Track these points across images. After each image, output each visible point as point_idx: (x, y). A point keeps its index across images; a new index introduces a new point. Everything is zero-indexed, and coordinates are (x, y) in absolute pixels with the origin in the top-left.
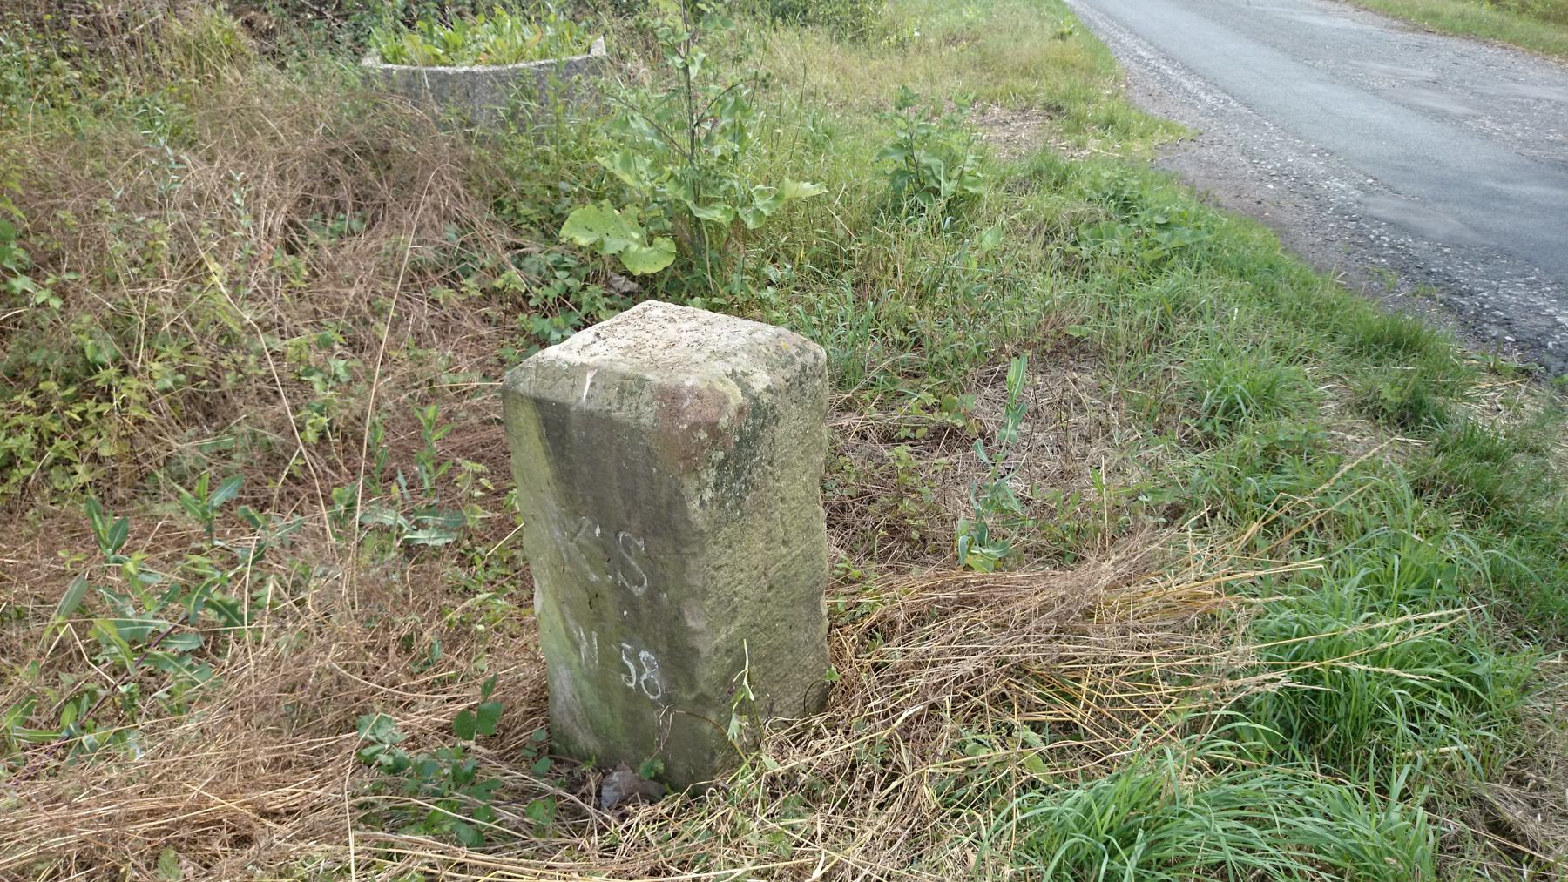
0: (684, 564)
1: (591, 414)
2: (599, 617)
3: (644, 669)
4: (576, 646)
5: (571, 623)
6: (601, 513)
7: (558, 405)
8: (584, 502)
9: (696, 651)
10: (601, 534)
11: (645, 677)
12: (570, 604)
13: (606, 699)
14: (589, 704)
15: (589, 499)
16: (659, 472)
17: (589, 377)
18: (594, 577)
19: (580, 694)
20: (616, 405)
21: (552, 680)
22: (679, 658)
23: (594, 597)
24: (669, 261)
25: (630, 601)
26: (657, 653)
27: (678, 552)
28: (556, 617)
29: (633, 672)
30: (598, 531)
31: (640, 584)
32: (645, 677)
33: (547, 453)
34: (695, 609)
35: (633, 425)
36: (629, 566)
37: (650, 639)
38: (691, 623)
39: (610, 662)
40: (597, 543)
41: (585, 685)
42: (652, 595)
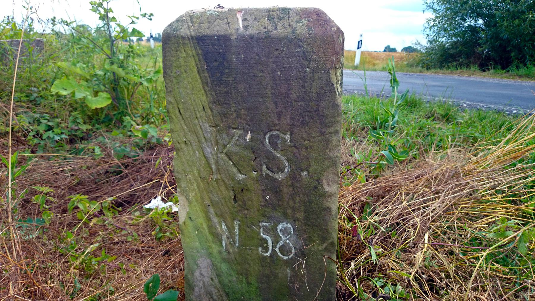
0: (327, 142)
1: (252, 37)
2: (244, 206)
3: (282, 237)
4: (217, 237)
5: (215, 220)
6: (256, 123)
7: (220, 37)
8: (239, 116)
9: (328, 210)
10: (251, 139)
11: (281, 243)
12: (213, 203)
13: (244, 273)
14: (226, 281)
15: (243, 112)
16: (312, 70)
17: (239, 16)
18: (240, 177)
19: (218, 275)
20: (270, 27)
21: (192, 272)
22: (312, 217)
23: (239, 193)
24: (109, 102)
25: (273, 187)
26: (294, 220)
27: (323, 134)
28: (201, 221)
29: (270, 243)
30: (249, 136)
31: (282, 170)
32: (281, 243)
33: (204, 83)
34: (331, 176)
35: (291, 36)
36: (275, 158)
37: (289, 211)
38: (327, 189)
39: (250, 239)
40: (246, 147)
41: (224, 267)
42: (294, 177)
